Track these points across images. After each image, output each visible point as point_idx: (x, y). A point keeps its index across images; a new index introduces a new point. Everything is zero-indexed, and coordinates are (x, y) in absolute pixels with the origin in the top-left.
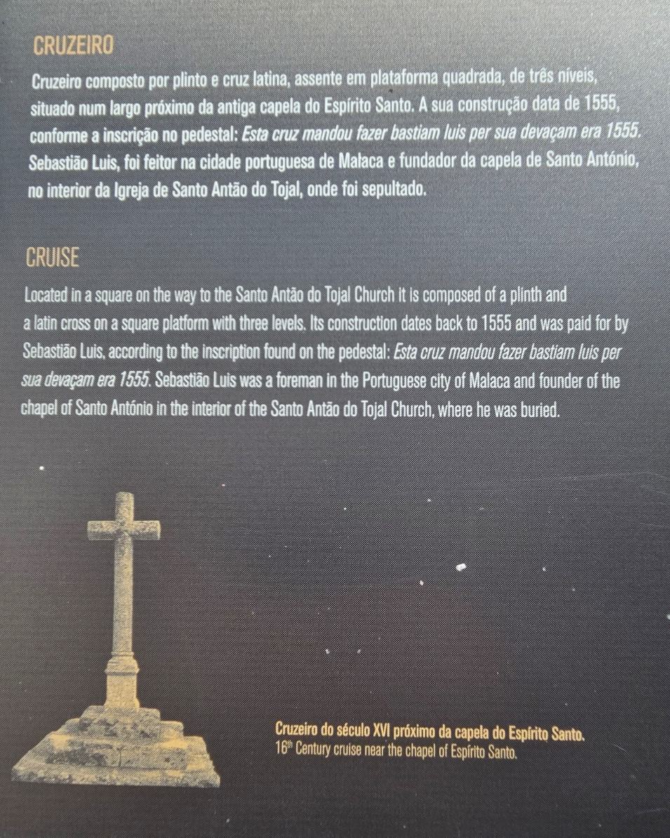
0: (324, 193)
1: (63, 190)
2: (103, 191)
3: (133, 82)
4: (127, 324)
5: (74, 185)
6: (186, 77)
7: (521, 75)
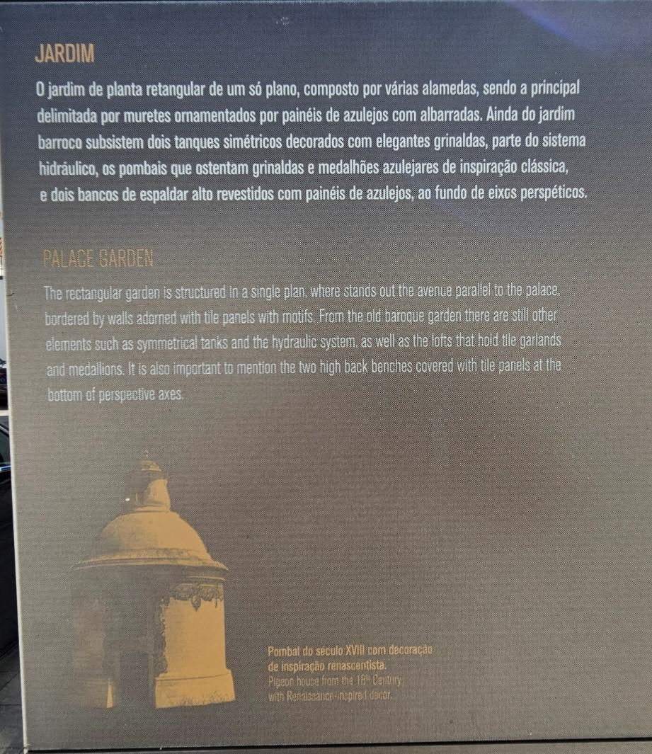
0: (256, 197)
1: (212, 168)
2: (177, 195)
3: (348, 89)
4: (255, 90)
5: (542, 82)
6: (72, 87)
7: (481, 192)
